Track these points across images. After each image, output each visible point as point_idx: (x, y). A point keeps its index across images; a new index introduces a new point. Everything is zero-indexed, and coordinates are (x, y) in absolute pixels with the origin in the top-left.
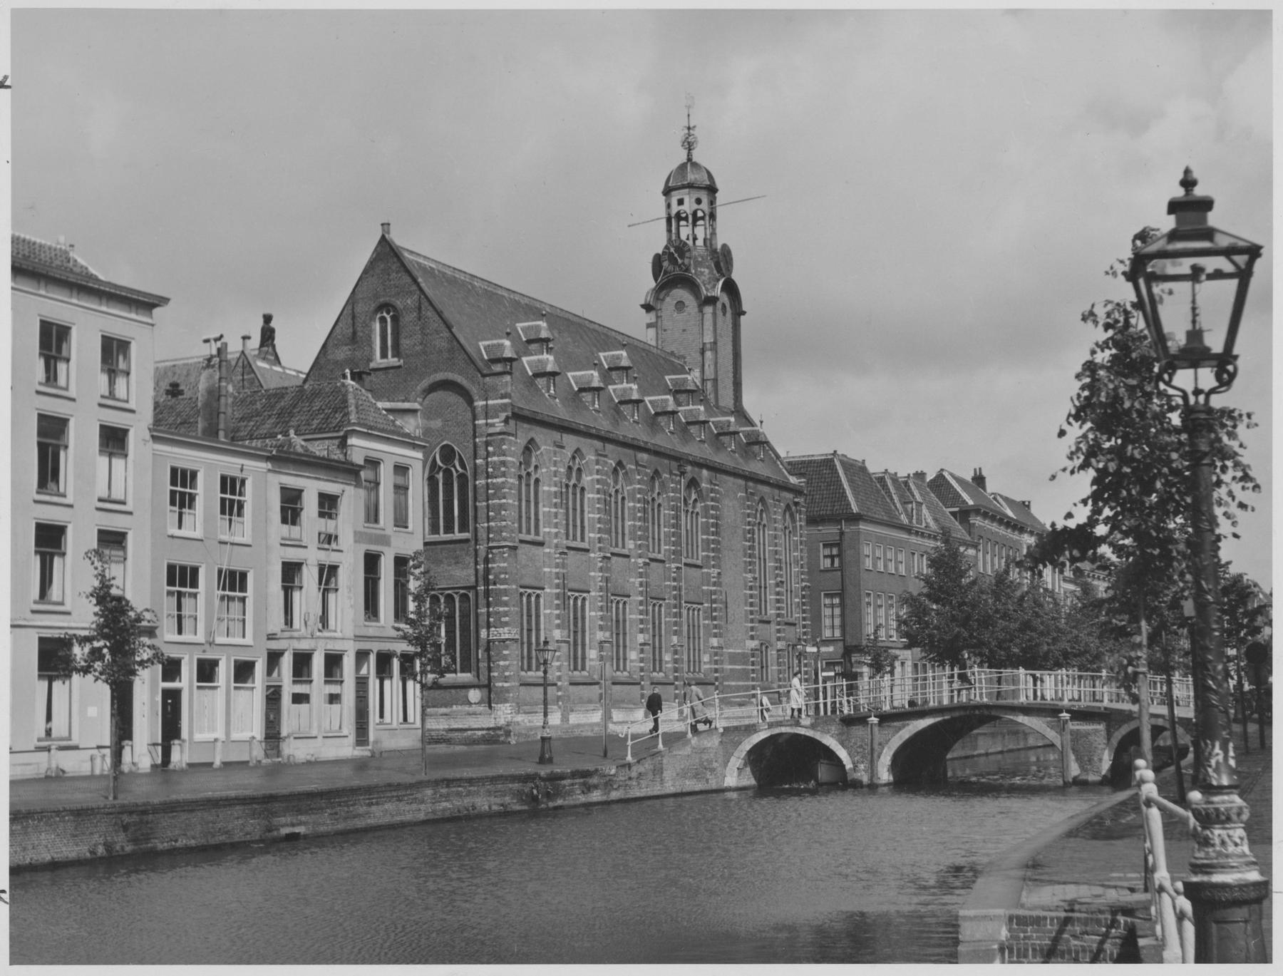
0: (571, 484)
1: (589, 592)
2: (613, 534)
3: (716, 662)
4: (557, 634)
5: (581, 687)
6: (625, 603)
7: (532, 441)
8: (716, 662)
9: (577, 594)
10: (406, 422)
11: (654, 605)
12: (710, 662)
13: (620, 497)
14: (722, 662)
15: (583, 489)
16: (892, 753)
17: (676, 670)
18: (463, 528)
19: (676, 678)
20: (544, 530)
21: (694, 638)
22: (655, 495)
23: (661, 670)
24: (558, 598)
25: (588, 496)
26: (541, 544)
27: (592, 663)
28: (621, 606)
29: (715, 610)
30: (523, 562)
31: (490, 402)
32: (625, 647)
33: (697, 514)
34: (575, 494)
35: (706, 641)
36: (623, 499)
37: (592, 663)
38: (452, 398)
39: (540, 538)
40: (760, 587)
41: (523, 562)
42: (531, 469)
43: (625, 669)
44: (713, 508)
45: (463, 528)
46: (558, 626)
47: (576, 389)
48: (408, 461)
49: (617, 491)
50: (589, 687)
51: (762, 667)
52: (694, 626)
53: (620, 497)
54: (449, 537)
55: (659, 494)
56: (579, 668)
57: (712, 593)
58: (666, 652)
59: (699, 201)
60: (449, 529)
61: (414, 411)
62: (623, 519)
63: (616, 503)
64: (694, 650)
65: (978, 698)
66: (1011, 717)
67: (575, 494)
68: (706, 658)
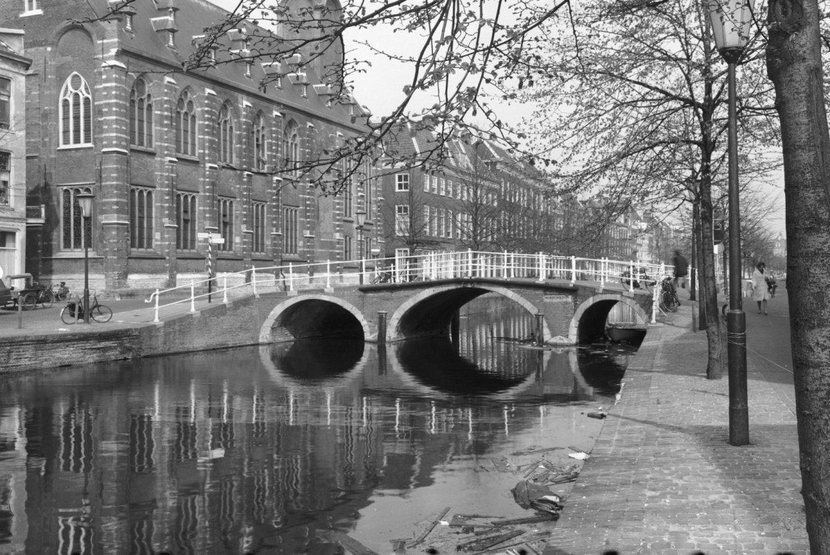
0: (183, 111)
1: (155, 187)
2: (222, 153)
3: (308, 247)
4: (113, 219)
5: (188, 261)
6: (231, 203)
7: (188, 87)
8: (308, 247)
9: (187, 193)
10: (12, 44)
11: (258, 205)
12: (304, 247)
13: (228, 126)
14: (313, 247)
15: (194, 117)
16: (284, 309)
17: (275, 251)
18: (87, 140)
19: (275, 257)
20: (155, 143)
21: (292, 230)
22: (260, 128)
23: (262, 251)
24: (168, 195)
25: (198, 122)
26: (153, 154)
27: (200, 244)
28: (260, 208)
29: (309, 211)
30: (136, 166)
31: (105, 41)
32: (296, 238)
33: (296, 145)
34: (186, 120)
35: (301, 232)
36: (231, 128)
37: (200, 244)
38: (79, 33)
39: (151, 150)
40: (346, 198)
41: (136, 166)
42: (145, 96)
43: (296, 252)
44: (308, 141)
45: (87, 140)
46: (245, 223)
47: (155, 30)
48: (11, 75)
49: (225, 122)
50: (196, 261)
51: (346, 252)
52: (291, 222)
53: (228, 126)
54: (78, 146)
55: (263, 128)
56: (137, 244)
57: (306, 200)
58: (267, 238)
60: (77, 141)
61: (20, 35)
62: (231, 143)
63: (225, 130)
64: (291, 238)
65: (505, 277)
66: (459, 287)
67: (186, 120)
68: (301, 243)
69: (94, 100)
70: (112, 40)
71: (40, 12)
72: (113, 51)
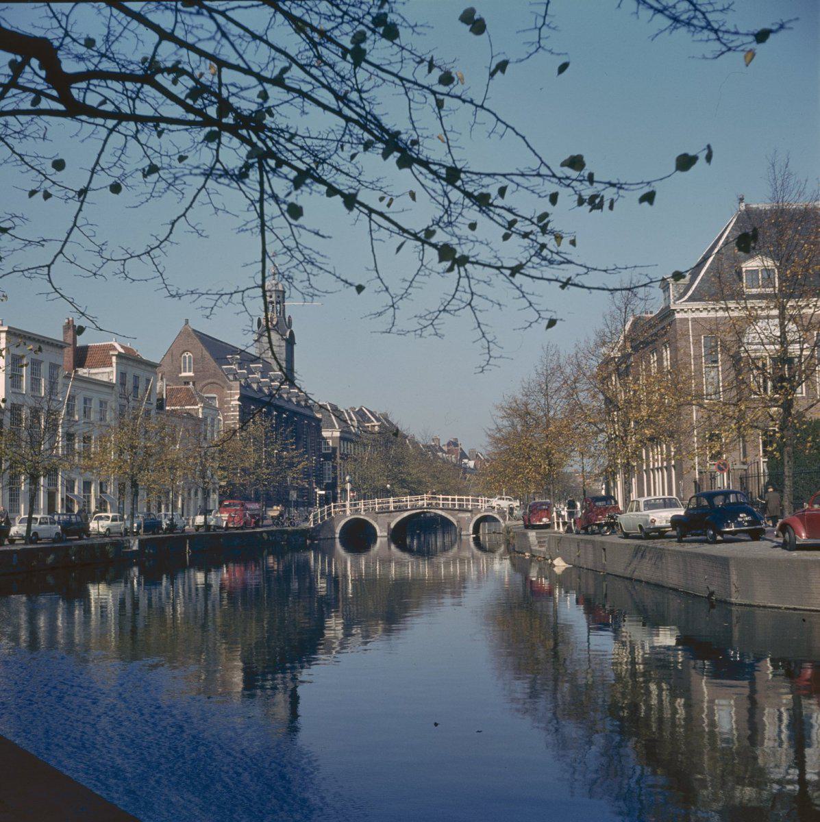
59: (279, 297)
69: (224, 421)
71: (191, 374)
72: (237, 397)
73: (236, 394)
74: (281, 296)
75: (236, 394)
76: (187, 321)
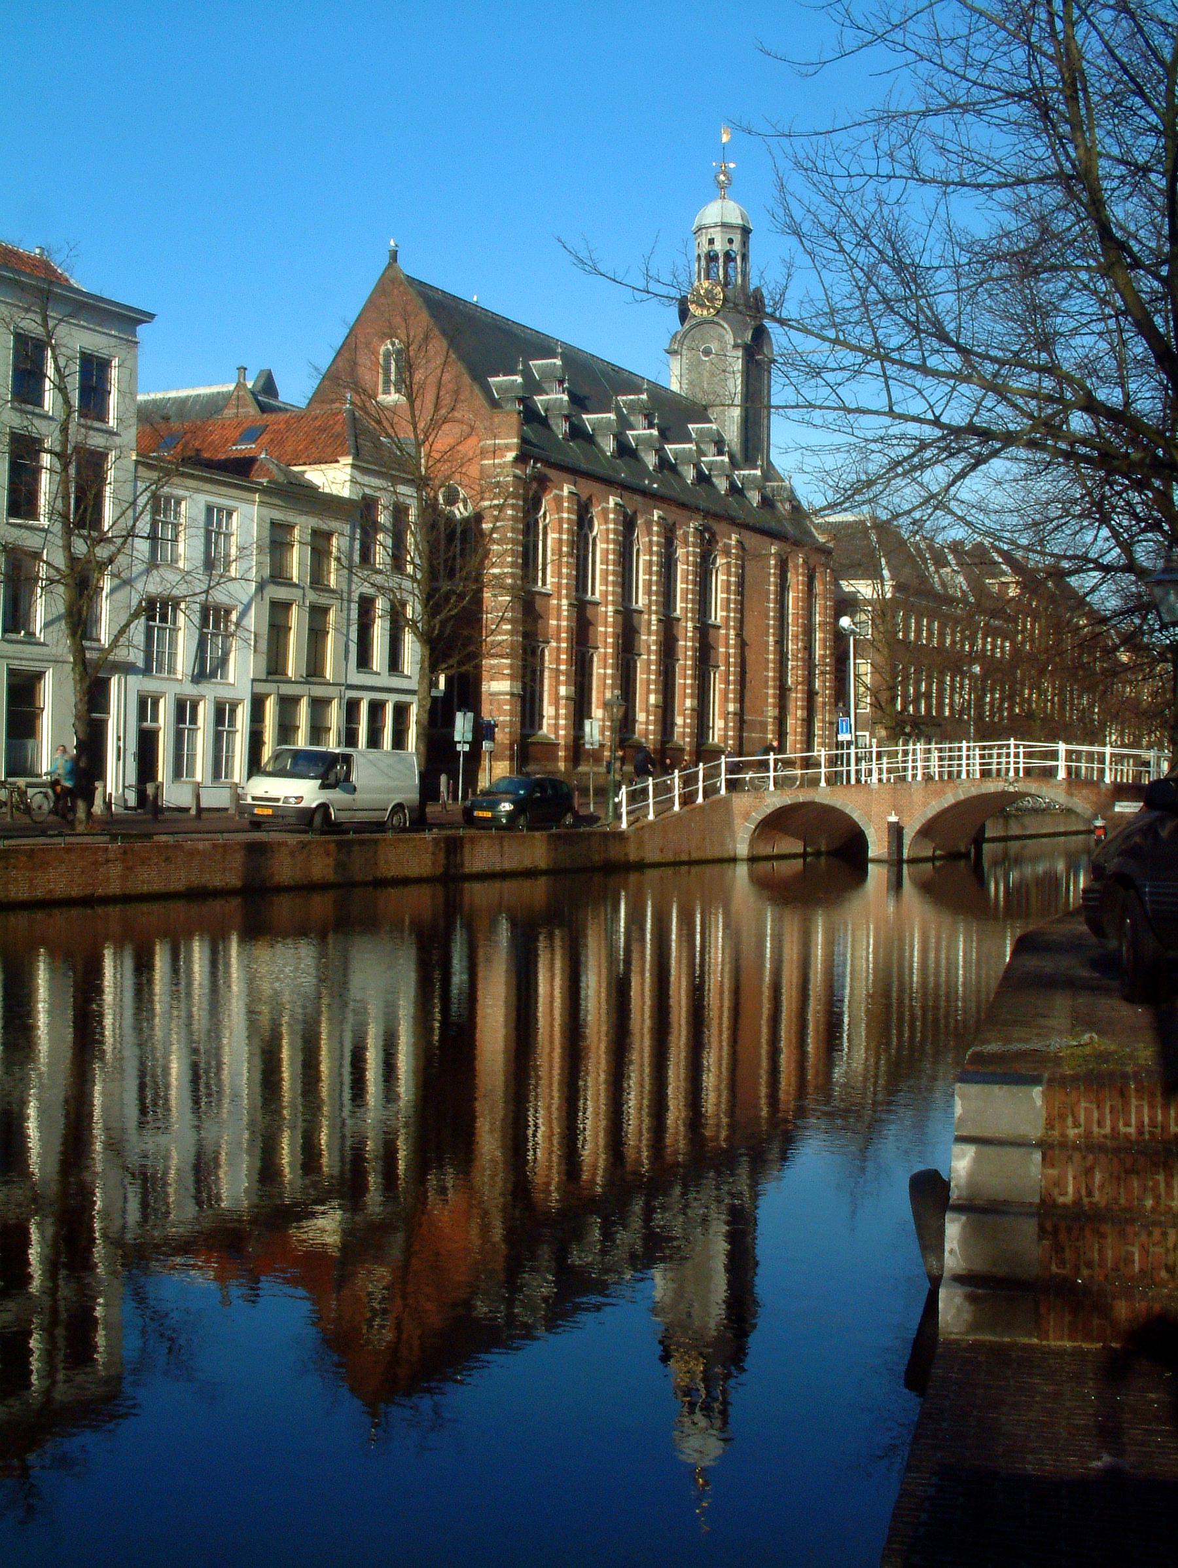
59: (731, 241)
70: (510, 441)
72: (510, 456)
73: (508, 448)
74: (737, 238)
75: (508, 448)
76: (394, 256)
